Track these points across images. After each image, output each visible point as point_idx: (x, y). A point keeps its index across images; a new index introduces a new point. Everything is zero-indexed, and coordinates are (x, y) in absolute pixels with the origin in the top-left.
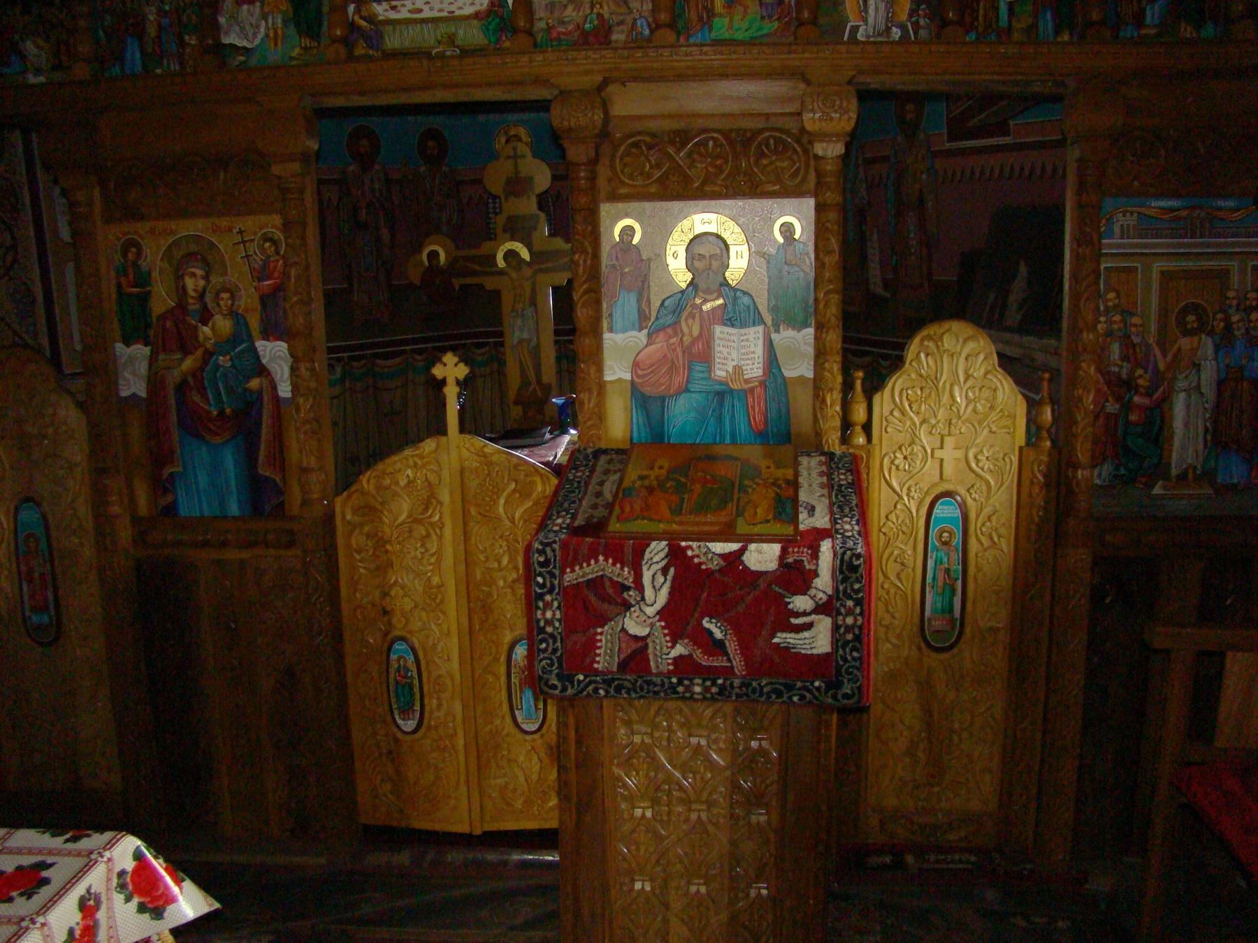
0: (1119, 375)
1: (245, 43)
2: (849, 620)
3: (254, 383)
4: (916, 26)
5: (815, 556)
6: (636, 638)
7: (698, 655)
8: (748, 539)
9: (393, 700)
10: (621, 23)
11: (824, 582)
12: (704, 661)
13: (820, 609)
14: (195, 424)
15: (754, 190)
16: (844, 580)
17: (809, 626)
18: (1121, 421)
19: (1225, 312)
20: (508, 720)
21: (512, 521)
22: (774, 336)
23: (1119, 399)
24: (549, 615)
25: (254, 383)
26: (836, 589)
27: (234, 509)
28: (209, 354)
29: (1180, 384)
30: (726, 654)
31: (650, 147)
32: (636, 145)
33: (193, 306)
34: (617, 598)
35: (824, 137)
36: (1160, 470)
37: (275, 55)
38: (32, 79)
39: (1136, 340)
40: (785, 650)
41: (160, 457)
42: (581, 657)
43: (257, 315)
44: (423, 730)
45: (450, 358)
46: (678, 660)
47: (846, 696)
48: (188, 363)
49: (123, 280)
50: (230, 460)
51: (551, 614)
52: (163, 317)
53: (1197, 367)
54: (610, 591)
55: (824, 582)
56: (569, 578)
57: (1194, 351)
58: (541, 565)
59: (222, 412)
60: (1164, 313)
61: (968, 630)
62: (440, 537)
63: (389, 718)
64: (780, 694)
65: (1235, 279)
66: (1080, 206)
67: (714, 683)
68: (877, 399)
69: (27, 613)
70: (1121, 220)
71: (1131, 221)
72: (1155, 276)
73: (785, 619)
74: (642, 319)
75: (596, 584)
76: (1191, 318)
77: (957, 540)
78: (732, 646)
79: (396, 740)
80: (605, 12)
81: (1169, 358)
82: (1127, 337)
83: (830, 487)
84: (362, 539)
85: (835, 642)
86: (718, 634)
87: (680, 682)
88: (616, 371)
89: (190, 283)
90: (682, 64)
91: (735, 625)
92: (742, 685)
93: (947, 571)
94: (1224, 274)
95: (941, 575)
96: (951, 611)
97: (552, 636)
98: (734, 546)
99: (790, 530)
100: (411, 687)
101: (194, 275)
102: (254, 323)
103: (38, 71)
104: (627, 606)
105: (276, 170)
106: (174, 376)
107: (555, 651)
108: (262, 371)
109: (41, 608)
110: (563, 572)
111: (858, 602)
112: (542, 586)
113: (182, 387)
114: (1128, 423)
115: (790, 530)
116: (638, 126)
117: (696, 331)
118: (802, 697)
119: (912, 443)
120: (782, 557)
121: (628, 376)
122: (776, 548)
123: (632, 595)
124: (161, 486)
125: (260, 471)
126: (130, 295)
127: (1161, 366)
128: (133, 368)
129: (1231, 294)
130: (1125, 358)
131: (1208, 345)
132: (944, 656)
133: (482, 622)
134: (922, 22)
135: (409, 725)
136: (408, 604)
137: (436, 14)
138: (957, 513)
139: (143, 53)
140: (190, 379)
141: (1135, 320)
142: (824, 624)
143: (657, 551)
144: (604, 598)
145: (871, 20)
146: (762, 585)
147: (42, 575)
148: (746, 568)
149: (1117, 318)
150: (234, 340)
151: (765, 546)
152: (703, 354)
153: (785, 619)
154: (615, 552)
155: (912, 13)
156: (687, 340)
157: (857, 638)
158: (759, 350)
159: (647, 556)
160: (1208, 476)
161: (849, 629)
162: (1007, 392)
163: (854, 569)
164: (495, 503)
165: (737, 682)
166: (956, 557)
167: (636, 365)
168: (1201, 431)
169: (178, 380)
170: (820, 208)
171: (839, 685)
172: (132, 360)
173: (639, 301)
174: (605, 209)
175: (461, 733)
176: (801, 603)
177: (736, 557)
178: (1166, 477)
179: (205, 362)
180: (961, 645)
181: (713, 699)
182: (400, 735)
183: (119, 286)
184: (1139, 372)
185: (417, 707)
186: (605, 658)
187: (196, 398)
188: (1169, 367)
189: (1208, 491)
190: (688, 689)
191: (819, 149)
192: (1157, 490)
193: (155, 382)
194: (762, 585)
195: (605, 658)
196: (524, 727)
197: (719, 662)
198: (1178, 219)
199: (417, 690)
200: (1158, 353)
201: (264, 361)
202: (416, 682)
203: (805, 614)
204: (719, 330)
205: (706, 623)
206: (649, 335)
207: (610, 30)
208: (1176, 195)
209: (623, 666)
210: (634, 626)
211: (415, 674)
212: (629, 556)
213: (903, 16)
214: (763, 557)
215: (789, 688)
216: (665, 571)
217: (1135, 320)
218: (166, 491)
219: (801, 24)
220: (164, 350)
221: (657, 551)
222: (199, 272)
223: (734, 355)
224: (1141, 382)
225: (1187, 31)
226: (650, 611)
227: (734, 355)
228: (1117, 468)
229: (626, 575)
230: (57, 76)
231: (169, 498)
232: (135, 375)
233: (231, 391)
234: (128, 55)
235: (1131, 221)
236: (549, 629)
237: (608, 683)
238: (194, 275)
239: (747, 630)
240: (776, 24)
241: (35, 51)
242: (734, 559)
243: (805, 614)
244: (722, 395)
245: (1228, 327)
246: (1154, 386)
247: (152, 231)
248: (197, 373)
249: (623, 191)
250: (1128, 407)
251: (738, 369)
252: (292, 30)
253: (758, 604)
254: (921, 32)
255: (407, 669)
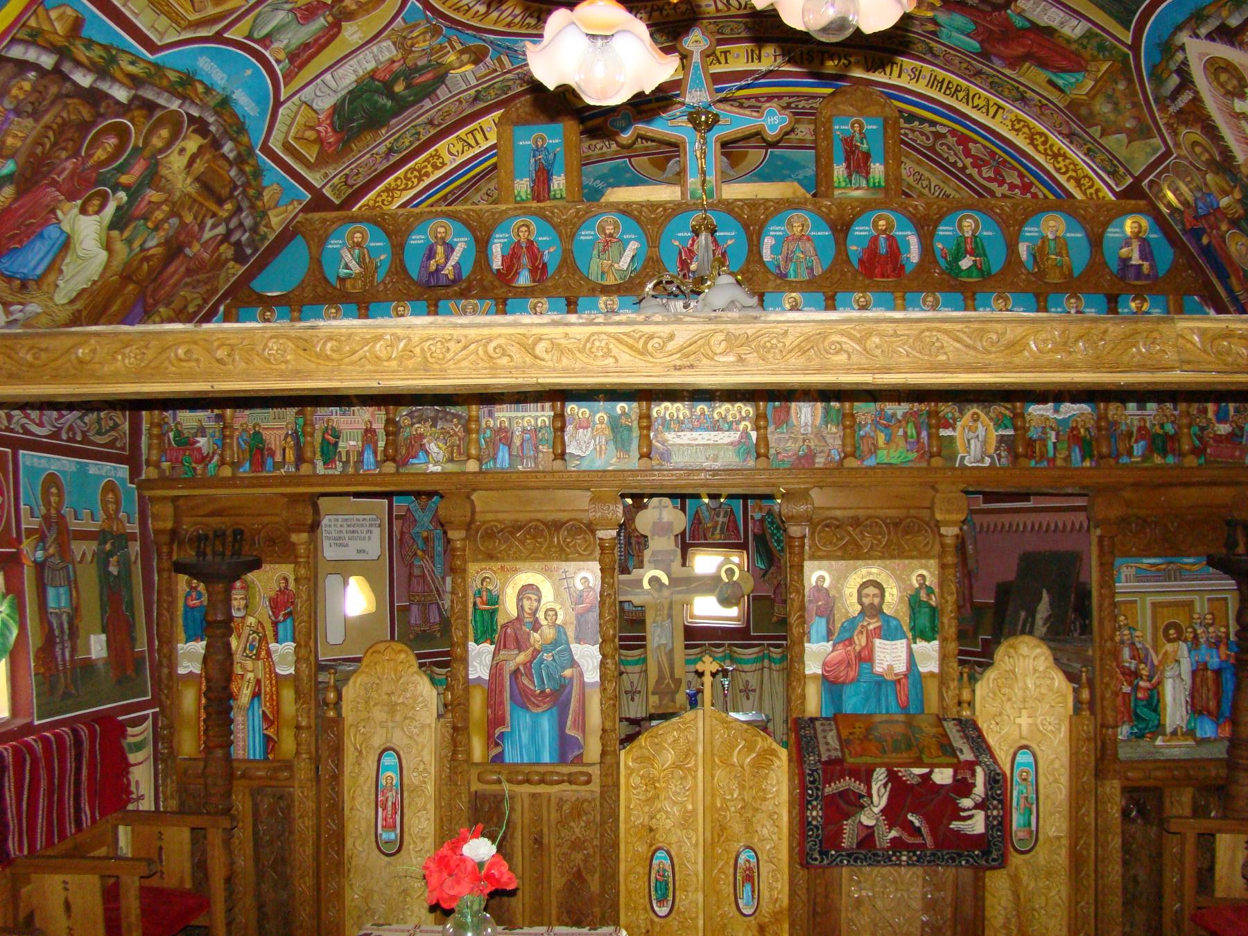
0: (1129, 668)
1: (580, 453)
2: (995, 813)
3: (568, 672)
4: (999, 455)
5: (974, 774)
6: (868, 827)
7: (905, 837)
8: (933, 766)
9: (653, 893)
10: (822, 452)
11: (979, 789)
12: (910, 840)
13: (978, 806)
14: (523, 699)
15: (902, 555)
16: (991, 789)
17: (970, 817)
18: (1133, 698)
19: (1191, 626)
20: (733, 906)
21: (742, 767)
22: (913, 646)
23: (1130, 684)
24: (814, 813)
25: (568, 672)
26: (986, 794)
27: (546, 758)
28: (536, 652)
29: (1168, 674)
30: (922, 835)
31: (838, 527)
32: (827, 526)
33: (528, 619)
34: (856, 802)
35: (948, 524)
36: (1159, 729)
37: (599, 464)
38: (432, 468)
39: (1139, 646)
40: (957, 833)
41: (495, 720)
42: (831, 840)
43: (573, 627)
44: (673, 914)
45: (707, 659)
46: (893, 840)
47: (994, 860)
48: (522, 658)
49: (478, 600)
50: (546, 724)
51: (815, 814)
52: (505, 626)
53: (1178, 662)
54: (852, 798)
55: (979, 789)
56: (828, 790)
57: (1175, 652)
58: (811, 782)
59: (543, 692)
60: (1155, 628)
61: (1041, 837)
62: (695, 778)
63: (648, 907)
64: (954, 860)
65: (1197, 608)
66: (1101, 564)
67: (915, 854)
68: (978, 686)
69: (380, 831)
70: (1125, 571)
71: (1132, 571)
72: (1148, 606)
73: (956, 813)
74: (829, 635)
75: (843, 794)
76: (1172, 631)
77: (1032, 778)
78: (924, 831)
79: (652, 922)
80: (812, 444)
81: (1160, 656)
82: (1133, 644)
83: (968, 739)
84: (638, 780)
85: (988, 826)
86: (917, 824)
87: (894, 854)
88: (813, 667)
89: (526, 604)
90: (622, 318)
91: (927, 818)
92: (933, 854)
93: (1026, 798)
94: (1190, 604)
95: (1022, 802)
96: (1030, 825)
97: (816, 827)
98: (926, 770)
99: (955, 761)
100: (667, 884)
101: (530, 598)
102: (571, 633)
103: (436, 463)
104: (862, 807)
105: (600, 534)
106: (511, 666)
107: (818, 836)
108: (573, 663)
109: (389, 827)
110: (824, 787)
111: (1000, 802)
112: (811, 796)
113: (516, 672)
114: (1137, 699)
115: (955, 761)
116: (828, 513)
117: (864, 643)
118: (967, 861)
119: (1001, 714)
120: (955, 776)
121: (819, 672)
122: (950, 771)
123: (865, 801)
124: (493, 740)
125: (568, 732)
126: (483, 610)
127: (1156, 663)
128: (480, 660)
129: (1196, 616)
130: (1133, 658)
131: (1183, 648)
132: (1027, 856)
133: (719, 836)
134: (1003, 454)
135: (663, 911)
136: (669, 823)
137: (705, 442)
138: (1031, 759)
139: (510, 455)
140: (521, 668)
141: (1138, 633)
142: (980, 816)
143: (880, 775)
144: (849, 803)
145: (972, 453)
146: (943, 792)
147: (394, 804)
148: (934, 783)
149: (1126, 632)
150: (555, 643)
151: (944, 770)
152: (866, 657)
153: (956, 813)
154: (855, 773)
155: (997, 448)
156: (858, 648)
157: (1000, 823)
158: (904, 655)
159: (875, 776)
160: (1190, 733)
161: (995, 818)
162: (1059, 680)
163: (996, 781)
164: (731, 754)
165: (928, 853)
166: (1032, 789)
167: (825, 664)
168: (1183, 703)
169: (513, 668)
170: (943, 567)
171: (989, 852)
172: (479, 654)
173: (828, 623)
174: (808, 565)
175: (701, 916)
176: (966, 803)
177: (926, 777)
178: (1164, 734)
179: (534, 657)
180: (1037, 848)
181: (914, 865)
182: (656, 919)
183: (475, 604)
184: (1142, 666)
185: (671, 898)
186: (849, 837)
187: (525, 681)
188: (1160, 662)
189: (1191, 742)
190: (899, 858)
191: (943, 530)
192: (1159, 742)
193: (496, 670)
194: (943, 792)
195: (849, 837)
196: (745, 911)
197: (918, 841)
198: (1159, 570)
199: (671, 885)
200: (1152, 652)
201: (576, 658)
202: (671, 880)
203: (969, 809)
204: (877, 642)
205: (910, 817)
206: (834, 646)
207: (814, 456)
208: (1156, 556)
209: (860, 845)
210: (867, 820)
211: (670, 873)
212: (863, 774)
213: (991, 451)
214: (943, 776)
215: (960, 855)
216: (885, 785)
217: (1138, 633)
218: (497, 744)
219: (932, 456)
220: (505, 647)
221: (880, 775)
222: (534, 597)
223: (888, 657)
224: (1144, 672)
225: (1158, 460)
226: (876, 810)
227: (888, 657)
228: (1132, 728)
229: (860, 788)
230: (451, 467)
231: (498, 750)
232: (481, 663)
233: (550, 676)
234: (500, 454)
235: (1132, 571)
236: (814, 823)
237: (849, 855)
238: (530, 598)
239: (935, 821)
240: (915, 455)
241: (436, 450)
242: (926, 777)
243: (969, 809)
244: (880, 682)
245: (1196, 637)
246: (1150, 678)
247: (502, 568)
248: (528, 665)
249: (820, 553)
250: (1136, 688)
251: (890, 667)
252: (612, 446)
253: (941, 804)
254: (1003, 460)
255: (665, 870)
